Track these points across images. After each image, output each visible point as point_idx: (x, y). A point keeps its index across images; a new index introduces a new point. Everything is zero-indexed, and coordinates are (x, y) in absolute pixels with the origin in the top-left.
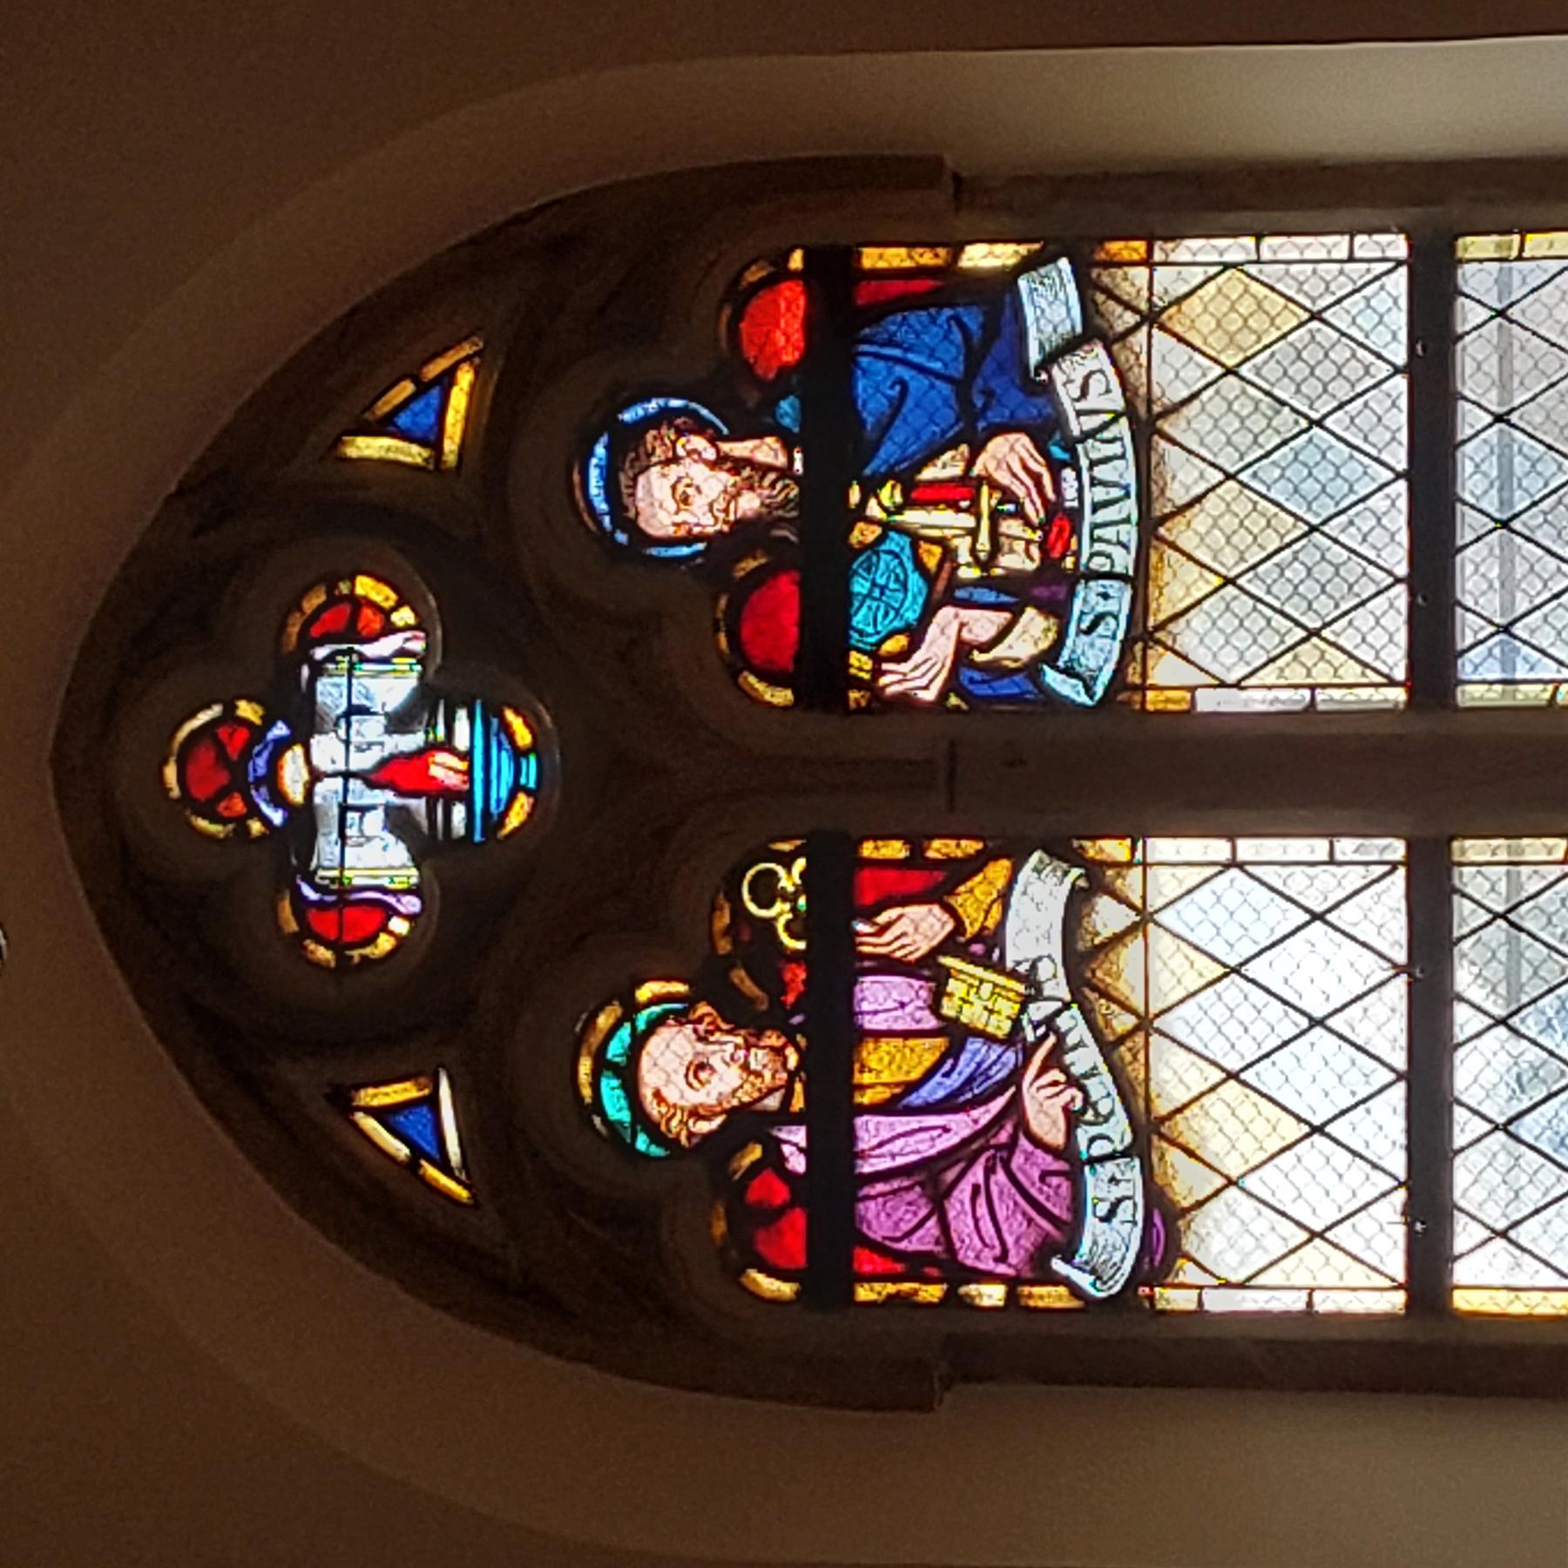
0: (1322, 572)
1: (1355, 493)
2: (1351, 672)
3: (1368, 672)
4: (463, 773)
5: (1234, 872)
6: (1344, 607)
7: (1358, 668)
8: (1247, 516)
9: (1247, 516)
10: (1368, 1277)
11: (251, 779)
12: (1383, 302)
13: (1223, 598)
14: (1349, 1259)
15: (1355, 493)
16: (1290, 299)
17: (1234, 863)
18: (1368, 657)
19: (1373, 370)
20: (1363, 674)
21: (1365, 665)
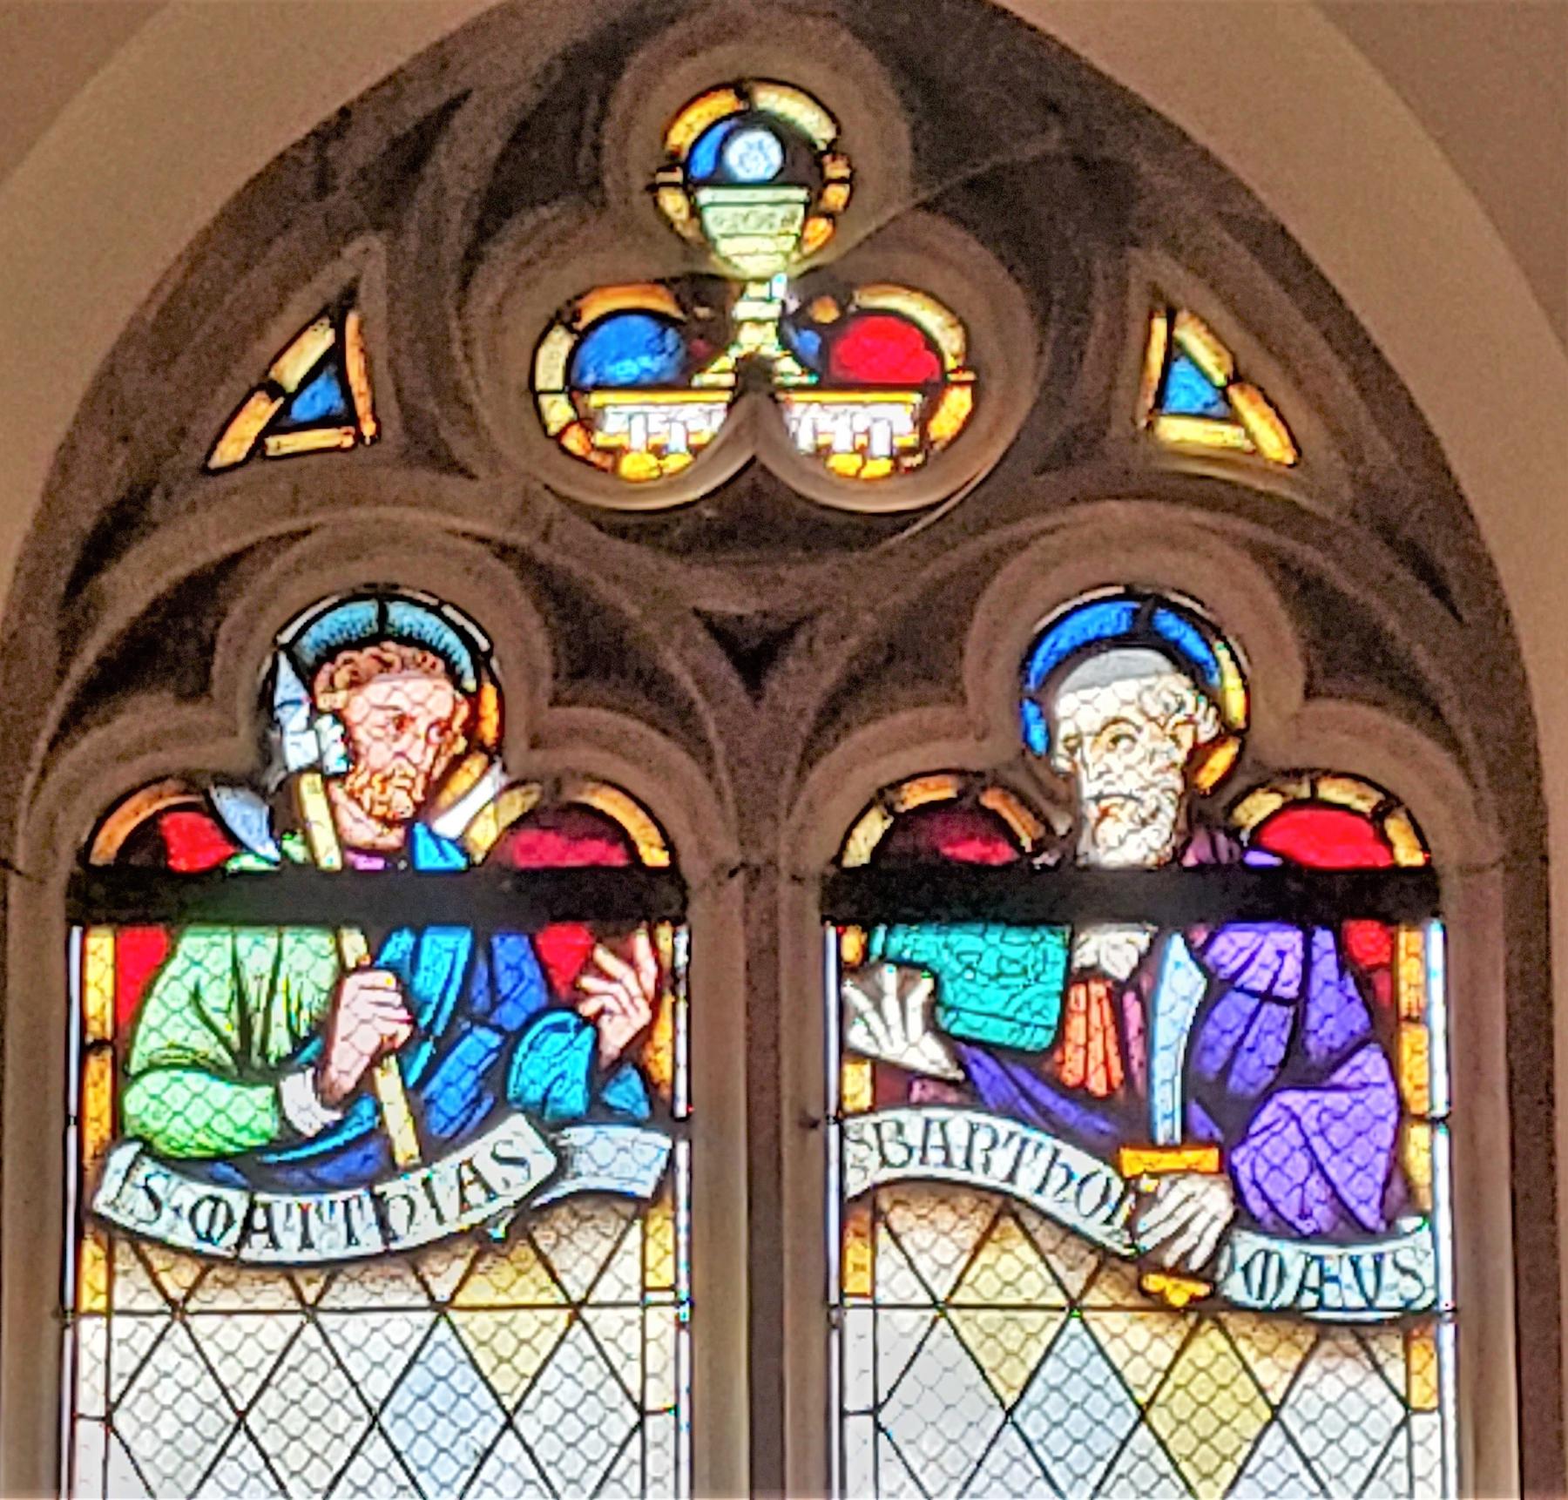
0: (315, 1404)
1: (1257, 1360)
2: (124, 1362)
3: (125, 1381)
4: (1319, 1339)
5: (120, 1419)
6: (1165, 1466)
7: (130, 1369)
8: (324, 1392)
9: (324, 1392)
10: (121, 1375)
11: (1447, 1332)
12: (1081, 1462)
13: (474, 1388)
14: (961, 1351)
15: (1257, 1360)
16: (1049, 1351)
17: (107, 1420)
18: (143, 1381)
19: (1208, 1484)
20: (121, 1375)
21: (133, 1378)
